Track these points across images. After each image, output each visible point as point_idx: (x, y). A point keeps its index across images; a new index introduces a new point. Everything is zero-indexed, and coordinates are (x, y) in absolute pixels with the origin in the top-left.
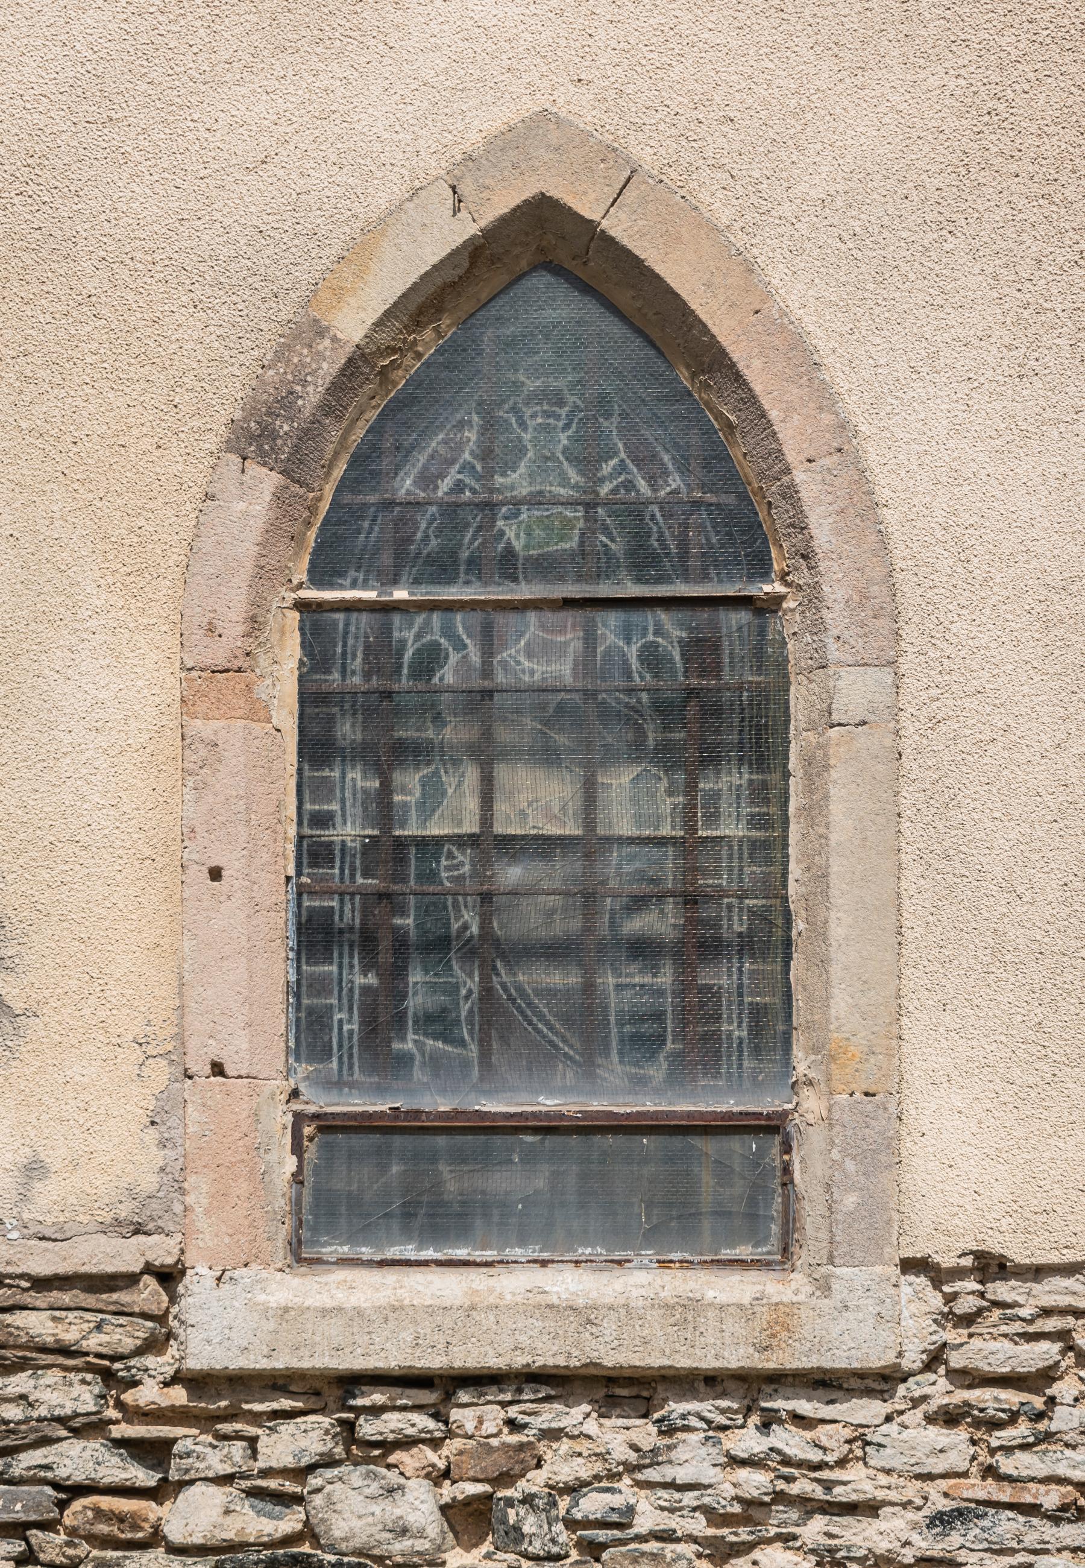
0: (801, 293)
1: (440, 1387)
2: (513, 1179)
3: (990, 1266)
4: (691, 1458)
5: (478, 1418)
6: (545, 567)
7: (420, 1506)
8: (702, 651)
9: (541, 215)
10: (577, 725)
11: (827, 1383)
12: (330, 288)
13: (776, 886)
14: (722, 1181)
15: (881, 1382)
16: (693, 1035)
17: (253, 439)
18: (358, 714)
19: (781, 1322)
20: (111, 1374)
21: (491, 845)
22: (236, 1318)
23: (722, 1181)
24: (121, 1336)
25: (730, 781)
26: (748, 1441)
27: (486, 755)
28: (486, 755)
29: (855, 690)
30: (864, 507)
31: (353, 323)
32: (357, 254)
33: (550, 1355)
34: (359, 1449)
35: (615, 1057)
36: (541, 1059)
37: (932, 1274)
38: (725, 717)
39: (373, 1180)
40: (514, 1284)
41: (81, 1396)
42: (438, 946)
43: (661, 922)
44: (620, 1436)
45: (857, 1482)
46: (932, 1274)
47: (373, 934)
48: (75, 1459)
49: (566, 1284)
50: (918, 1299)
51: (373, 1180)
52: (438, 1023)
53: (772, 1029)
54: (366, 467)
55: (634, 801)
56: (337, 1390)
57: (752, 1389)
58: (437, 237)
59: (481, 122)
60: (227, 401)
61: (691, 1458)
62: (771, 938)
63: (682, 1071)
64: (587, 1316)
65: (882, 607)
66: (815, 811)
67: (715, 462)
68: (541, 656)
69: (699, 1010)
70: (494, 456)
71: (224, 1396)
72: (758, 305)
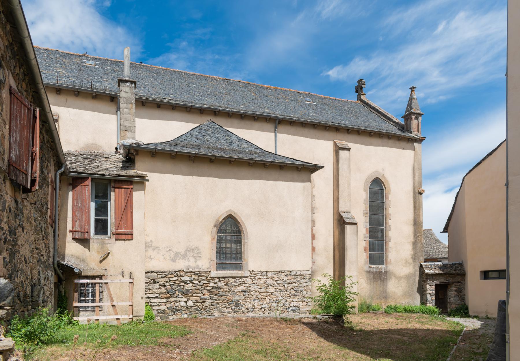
0: (243, 220)
1: (225, 278)
2: (228, 266)
3: (253, 271)
4: (238, 281)
5: (226, 279)
6: (229, 233)
7: (223, 284)
8: (237, 238)
9: (230, 215)
10: (231, 241)
11: (244, 277)
12: (219, 218)
13: (241, 250)
14: (239, 266)
15: (247, 277)
16: (236, 258)
17: (215, 226)
18: (220, 241)
19: (242, 274)
20: (206, 277)
21: (226, 248)
22: (214, 274)
23: (239, 266)
24: (207, 275)
25: (238, 245)
26: (240, 280)
27: (226, 243)
28: (226, 243)
29: (246, 241)
30: (247, 231)
31: (220, 220)
32: (221, 216)
33: (231, 276)
34: (220, 281)
35: (21, 193)
36: (228, 260)
37: (504, 306)
38: (239, 242)
39: (221, 266)
40: (228, 272)
41: (205, 278)
42: (223, 253)
43: (235, 252)
44: (234, 280)
45: (246, 282)
46: (504, 306)
47: (220, 253)
48: (205, 282)
49: (231, 272)
50: (249, 272)
51: (221, 266)
52: (223, 257)
53: (241, 258)
54: (220, 227)
55: (234, 246)
56: (219, 278)
57: (241, 277)
58: (225, 216)
59: (227, 209)
60: (213, 223)
61: (238, 281)
62: (241, 253)
63: (236, 260)
64: (233, 274)
65: (247, 236)
66: (244, 247)
67: (238, 228)
68: (229, 238)
69: (236, 257)
70: (226, 227)
71: (213, 278)
72: (241, 220)
